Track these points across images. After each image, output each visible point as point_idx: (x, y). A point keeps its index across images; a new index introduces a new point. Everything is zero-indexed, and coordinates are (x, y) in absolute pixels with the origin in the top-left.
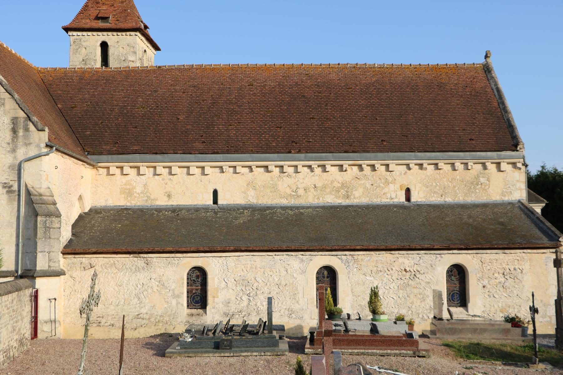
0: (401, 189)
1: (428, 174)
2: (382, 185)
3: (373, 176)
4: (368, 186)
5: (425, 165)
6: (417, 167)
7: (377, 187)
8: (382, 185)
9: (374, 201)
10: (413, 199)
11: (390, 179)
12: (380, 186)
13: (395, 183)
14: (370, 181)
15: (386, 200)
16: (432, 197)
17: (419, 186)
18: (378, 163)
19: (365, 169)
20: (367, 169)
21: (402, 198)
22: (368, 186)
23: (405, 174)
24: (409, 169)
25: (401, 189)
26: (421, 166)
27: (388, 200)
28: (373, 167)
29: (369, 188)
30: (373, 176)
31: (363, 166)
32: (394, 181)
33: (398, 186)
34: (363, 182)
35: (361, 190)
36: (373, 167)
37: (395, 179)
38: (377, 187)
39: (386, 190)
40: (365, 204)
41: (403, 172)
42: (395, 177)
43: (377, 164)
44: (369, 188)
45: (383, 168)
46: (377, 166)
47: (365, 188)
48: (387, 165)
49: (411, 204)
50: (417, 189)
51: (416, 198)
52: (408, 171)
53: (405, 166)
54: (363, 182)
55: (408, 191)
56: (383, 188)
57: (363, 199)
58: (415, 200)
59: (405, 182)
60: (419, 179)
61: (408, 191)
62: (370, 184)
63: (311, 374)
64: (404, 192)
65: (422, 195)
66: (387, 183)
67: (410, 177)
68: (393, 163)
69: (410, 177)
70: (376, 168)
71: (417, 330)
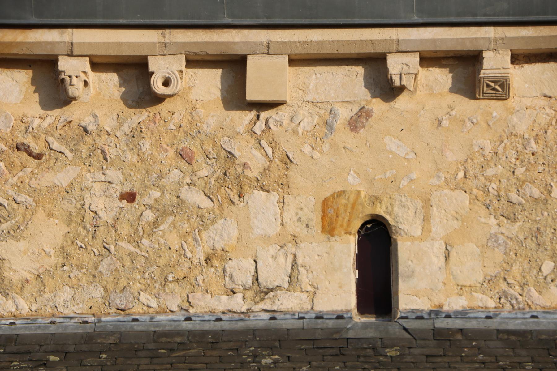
0: (329, 229)
1: (522, 126)
2: (195, 198)
3: (135, 135)
4: (104, 204)
5: (495, 63)
6: (442, 77)
7: (162, 212)
8: (195, 198)
9: (137, 309)
10: (412, 296)
11: (254, 159)
12: (181, 203)
13: (284, 185)
14: (113, 174)
15: (222, 303)
16: (543, 285)
17: (453, 203)
18: (166, 50)
19: (76, 88)
20: (98, 95)
21: (336, 291)
22: (105, 205)
23: (354, 124)
24: (387, 89)
25: (329, 229)
26: (465, 66)
27: (238, 303)
28: (134, 71)
29: (106, 217)
30: (135, 135)
31: (65, 65)
32: (278, 176)
33: (305, 205)
34: (62, 178)
35: (49, 233)
36: (134, 71)
37: (287, 161)
38: (162, 212)
39: (224, 233)
40: (72, 326)
41: (345, 113)
42: (288, 145)
43: (165, 53)
44: (106, 217)
45: (210, 81)
46: (160, 67)
47: (83, 219)
48: (234, 66)
49: (394, 329)
50: (438, 229)
51: (427, 285)
52: (378, 106)
53: (359, 71)
54: (62, 178)
55: (377, 244)
56: (205, 221)
57: (66, 294)
58: (423, 305)
59: (353, 181)
60: (454, 156)
61: (377, 244)
62: (118, 189)
63: (3, 368)
64: (348, 247)
65: (471, 266)
66: (232, 183)
67: (392, 144)
68: (268, 49)
69: (392, 144)
70: (157, 86)
71: (41, 214)
